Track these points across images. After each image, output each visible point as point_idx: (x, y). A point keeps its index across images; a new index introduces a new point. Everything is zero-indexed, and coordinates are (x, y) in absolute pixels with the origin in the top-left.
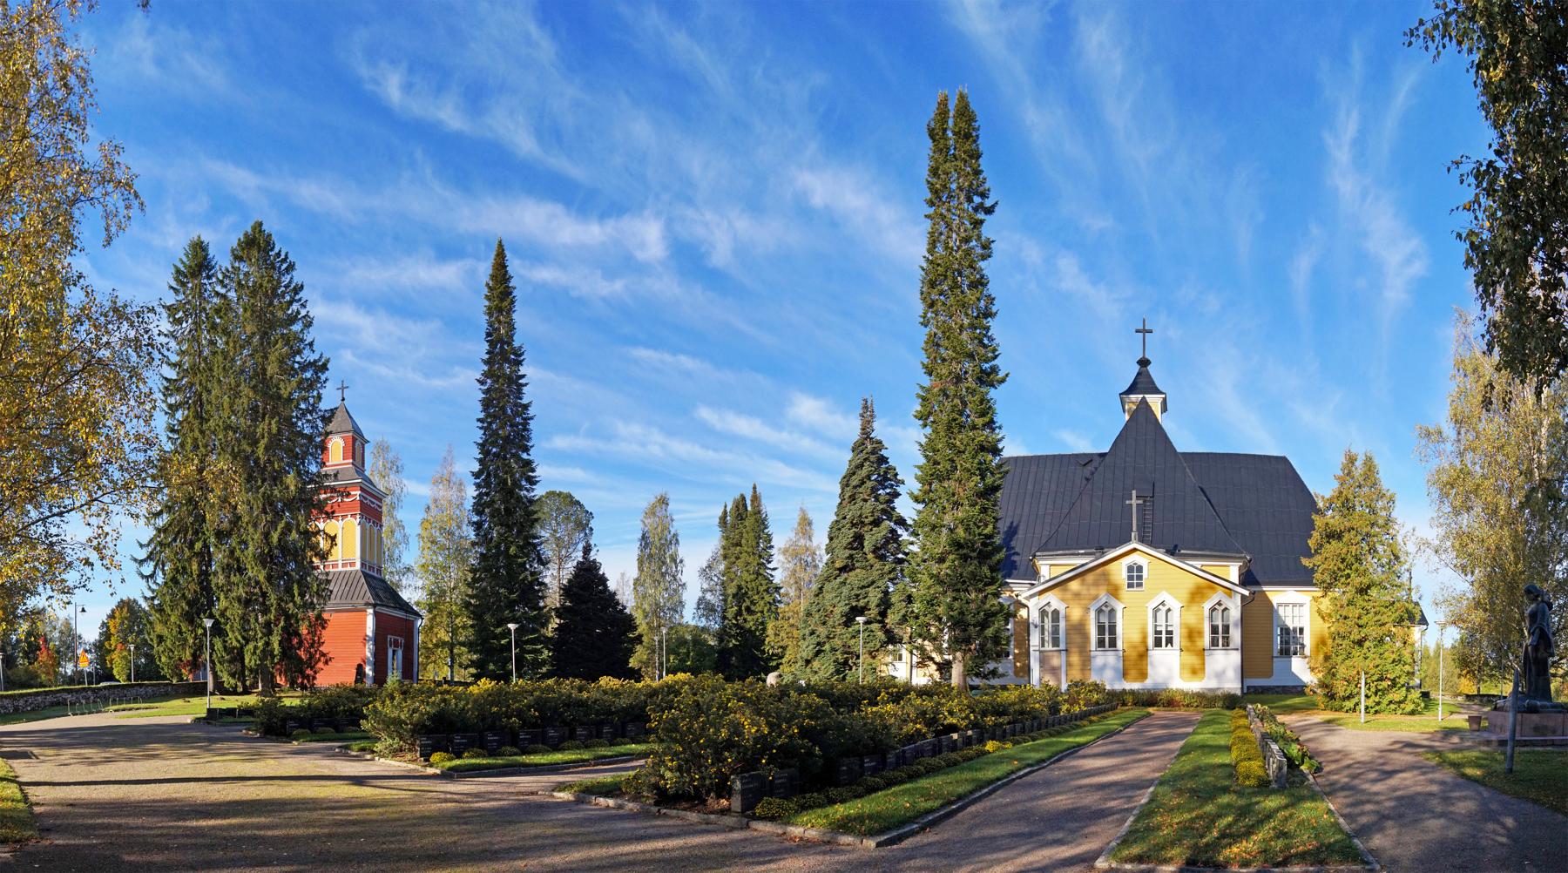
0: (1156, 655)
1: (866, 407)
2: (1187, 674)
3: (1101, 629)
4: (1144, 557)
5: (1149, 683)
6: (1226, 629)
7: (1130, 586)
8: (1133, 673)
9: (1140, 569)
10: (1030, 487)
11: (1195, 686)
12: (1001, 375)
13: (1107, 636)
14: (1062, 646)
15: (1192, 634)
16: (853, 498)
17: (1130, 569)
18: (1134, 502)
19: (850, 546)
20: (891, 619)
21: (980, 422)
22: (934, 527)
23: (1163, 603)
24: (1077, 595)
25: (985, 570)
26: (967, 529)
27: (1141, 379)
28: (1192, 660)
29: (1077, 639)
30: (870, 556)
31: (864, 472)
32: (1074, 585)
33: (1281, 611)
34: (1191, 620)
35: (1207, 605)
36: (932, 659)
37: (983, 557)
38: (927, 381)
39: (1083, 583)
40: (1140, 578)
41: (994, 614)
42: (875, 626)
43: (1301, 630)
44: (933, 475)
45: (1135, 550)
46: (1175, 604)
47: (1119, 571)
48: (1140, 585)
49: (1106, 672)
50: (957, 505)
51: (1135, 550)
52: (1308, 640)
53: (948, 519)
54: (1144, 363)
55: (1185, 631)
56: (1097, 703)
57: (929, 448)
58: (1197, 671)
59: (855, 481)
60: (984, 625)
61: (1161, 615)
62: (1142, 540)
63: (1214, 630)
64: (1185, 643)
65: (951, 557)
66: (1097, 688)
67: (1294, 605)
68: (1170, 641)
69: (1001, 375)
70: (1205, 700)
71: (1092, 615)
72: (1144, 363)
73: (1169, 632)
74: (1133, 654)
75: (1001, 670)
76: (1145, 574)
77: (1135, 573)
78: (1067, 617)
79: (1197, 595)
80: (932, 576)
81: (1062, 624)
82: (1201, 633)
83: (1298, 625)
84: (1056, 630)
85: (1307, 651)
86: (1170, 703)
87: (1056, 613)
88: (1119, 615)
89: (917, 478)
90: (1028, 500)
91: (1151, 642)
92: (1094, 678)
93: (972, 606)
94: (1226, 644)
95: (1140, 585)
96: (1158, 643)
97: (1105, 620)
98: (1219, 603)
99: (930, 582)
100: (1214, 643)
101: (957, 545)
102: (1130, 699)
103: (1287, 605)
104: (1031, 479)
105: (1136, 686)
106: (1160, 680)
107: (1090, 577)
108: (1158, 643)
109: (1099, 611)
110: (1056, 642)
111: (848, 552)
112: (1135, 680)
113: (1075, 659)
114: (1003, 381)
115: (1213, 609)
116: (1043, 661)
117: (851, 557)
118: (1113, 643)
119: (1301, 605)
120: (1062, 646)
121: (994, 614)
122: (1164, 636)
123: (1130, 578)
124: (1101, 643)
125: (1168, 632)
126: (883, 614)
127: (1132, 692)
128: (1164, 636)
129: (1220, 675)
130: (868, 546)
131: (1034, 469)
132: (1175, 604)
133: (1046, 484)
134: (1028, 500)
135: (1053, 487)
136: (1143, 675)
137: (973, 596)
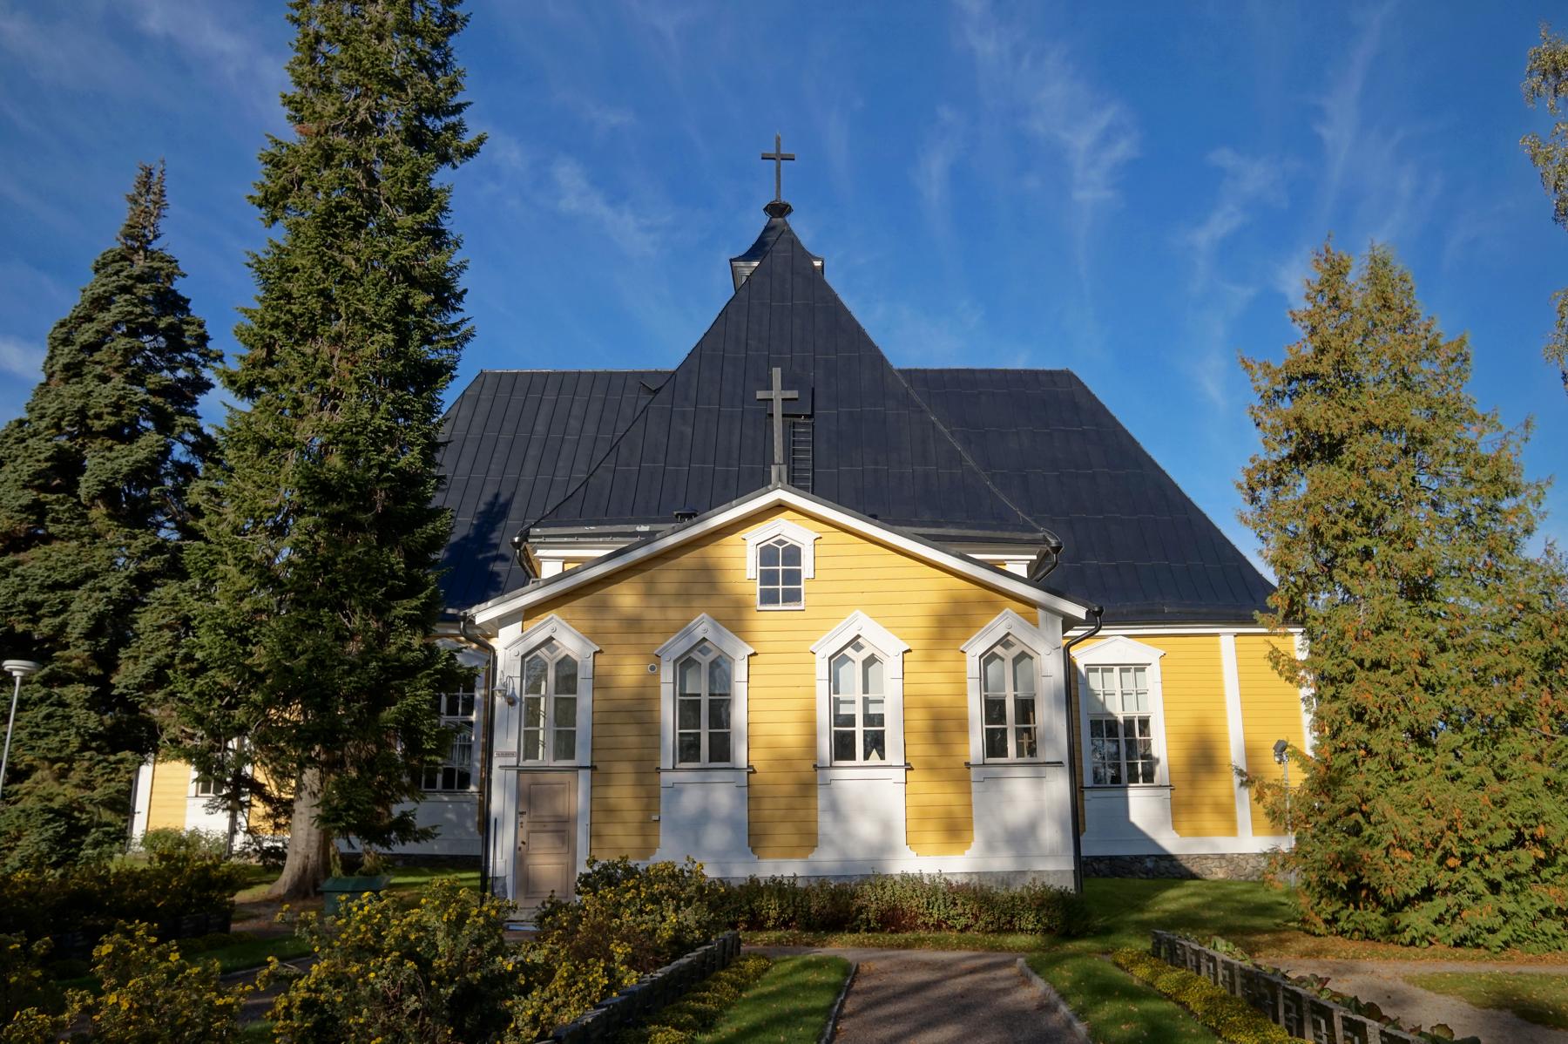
0: (852, 779)
1: (146, 184)
2: (932, 837)
3: (689, 709)
4: (801, 524)
5: (826, 860)
6: (1026, 708)
7: (769, 598)
8: (784, 834)
9: (793, 554)
10: (540, 428)
11: (955, 864)
12: (467, 139)
13: (709, 731)
14: (582, 756)
15: (941, 726)
16: (73, 371)
17: (768, 555)
18: (777, 394)
19: (40, 481)
20: (127, 675)
21: (405, 221)
22: (265, 446)
23: (855, 643)
24: (633, 624)
25: (397, 560)
26: (351, 454)
27: (772, 237)
28: (939, 795)
29: (630, 736)
30: (98, 512)
31: (108, 317)
32: (626, 597)
33: (1095, 681)
34: (936, 685)
35: (977, 646)
36: (257, 789)
37: (392, 527)
38: (291, 134)
39: (649, 593)
40: (793, 577)
41: (410, 671)
42: (74, 693)
43: (1144, 723)
44: (288, 324)
45: (780, 507)
46: (886, 643)
47: (742, 559)
48: (793, 596)
49: (700, 830)
50: (331, 398)
51: (780, 507)
52: (1160, 745)
53: (304, 431)
54: (778, 210)
55: (919, 719)
56: (679, 944)
57: (277, 274)
58: (955, 830)
59: (86, 334)
60: (379, 695)
61: (851, 675)
62: (795, 481)
63: (994, 709)
64: (919, 750)
65: (307, 521)
66: (678, 886)
67: (1125, 668)
68: (876, 742)
69: (467, 139)
70: (987, 907)
71: (667, 675)
72: (778, 210)
73: (874, 720)
74: (784, 784)
75: (420, 823)
76: (806, 568)
77: (782, 571)
78: (600, 683)
79: (951, 624)
80: (246, 565)
81: (584, 699)
82: (963, 726)
83: (1133, 712)
84: (565, 711)
85: (1161, 772)
86: (892, 920)
87: (567, 673)
88: (740, 672)
89: (239, 333)
90: (533, 452)
91: (825, 746)
92: (668, 852)
93: (353, 647)
94: (1029, 747)
95: (793, 596)
96: (844, 747)
97: (699, 686)
98: (1005, 642)
99: (244, 581)
100: (995, 745)
101: (319, 488)
102: (772, 908)
103: (1107, 668)
104: (545, 409)
105: (789, 868)
106: (859, 854)
107: (668, 578)
108: (844, 747)
109: (685, 664)
110: (565, 744)
111: (28, 496)
112: (791, 852)
113: (623, 793)
114: (470, 152)
115: (988, 658)
116: (527, 799)
117: (37, 508)
118: (721, 750)
119: (1140, 668)
120: (582, 756)
121: (410, 671)
122: (859, 729)
123: (767, 577)
124: (689, 749)
125: (870, 719)
126: (108, 662)
127: (779, 888)
128: (859, 729)
129: (1021, 838)
130: (87, 485)
131: (550, 396)
132: (886, 643)
133: (574, 423)
134: (533, 452)
135: (590, 429)
136: (809, 840)
137: (357, 621)
